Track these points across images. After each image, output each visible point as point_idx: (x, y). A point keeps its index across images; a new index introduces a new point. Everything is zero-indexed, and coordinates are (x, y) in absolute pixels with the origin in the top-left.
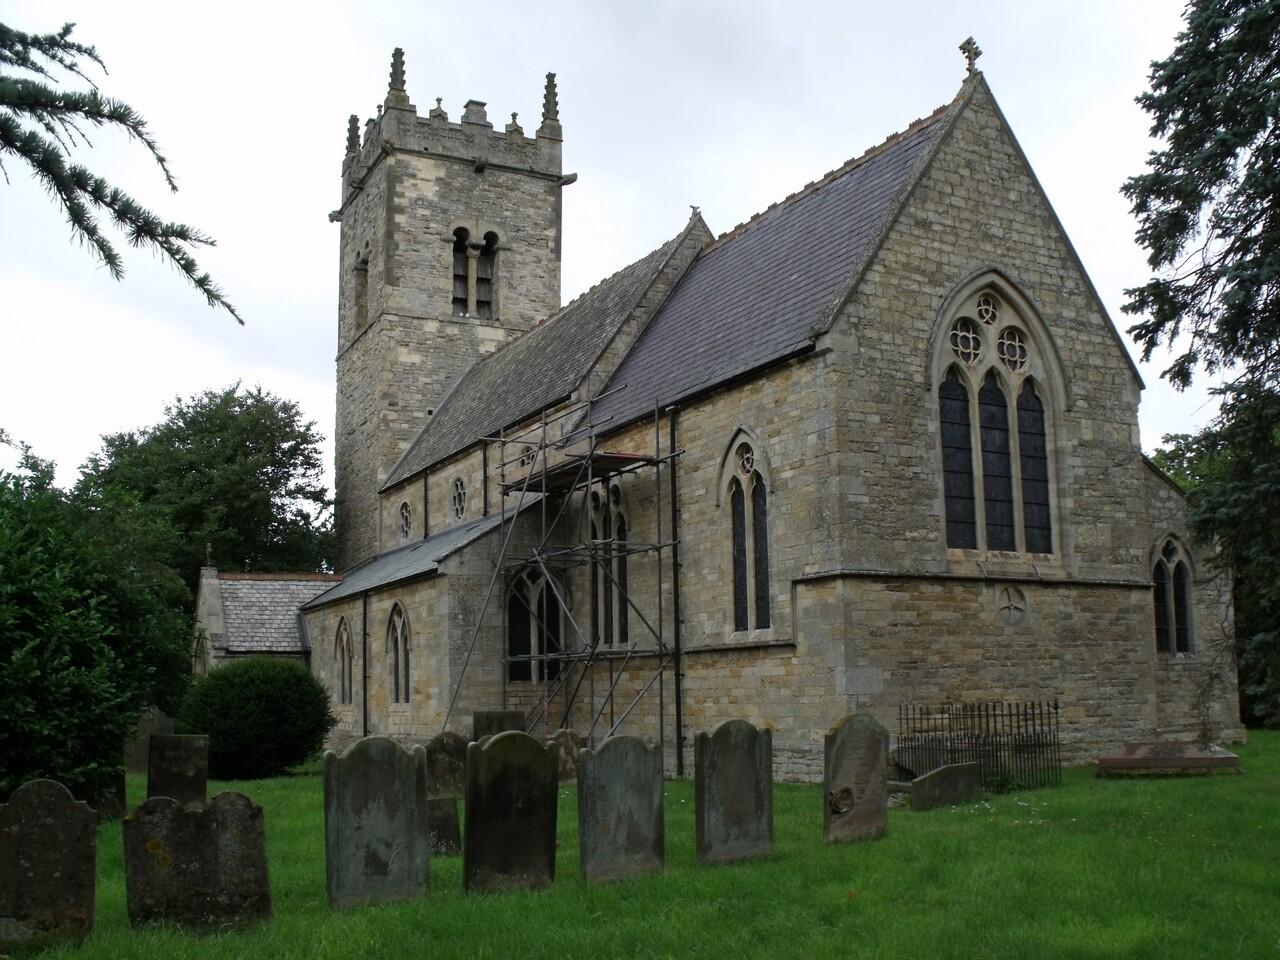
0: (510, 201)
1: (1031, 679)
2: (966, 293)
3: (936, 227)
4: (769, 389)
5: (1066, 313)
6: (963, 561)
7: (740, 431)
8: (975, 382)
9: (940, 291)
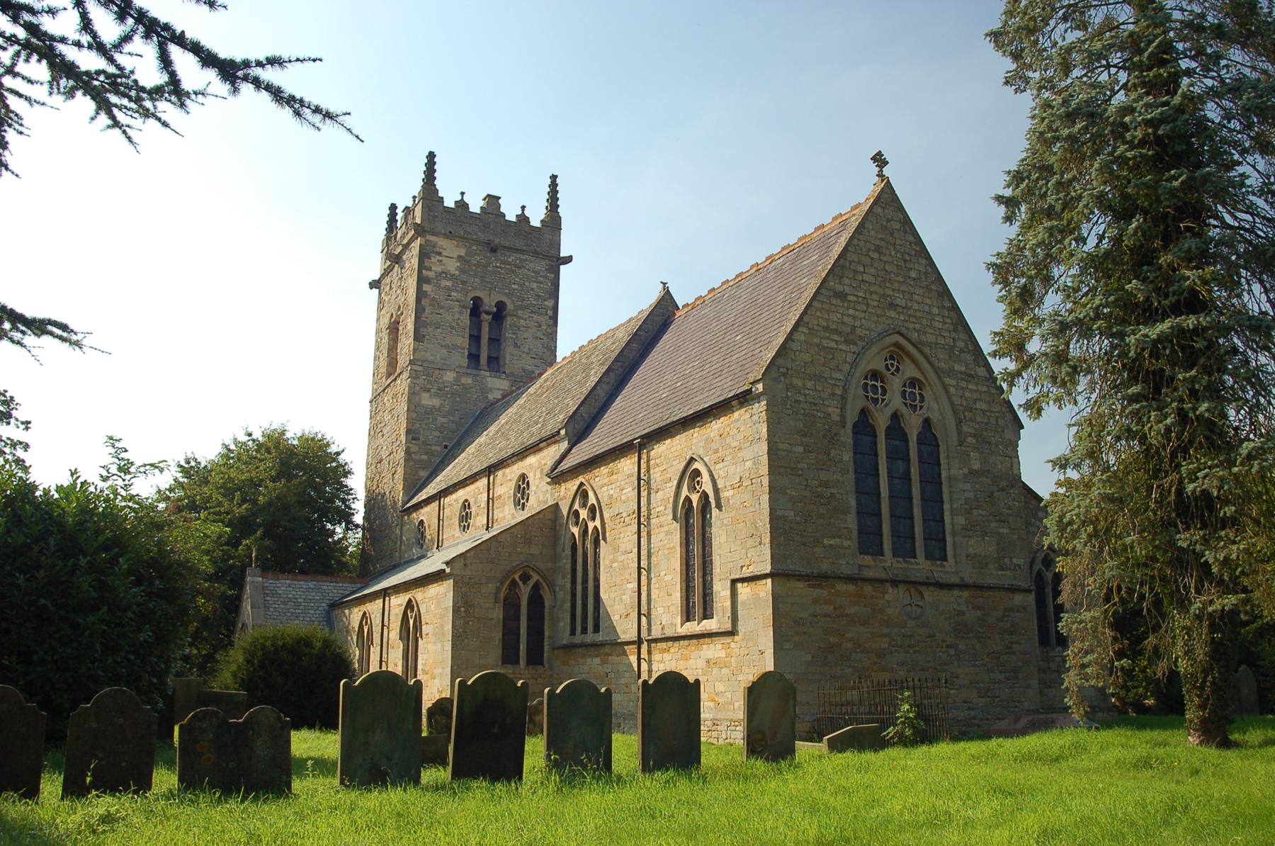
2: (874, 350)
3: (851, 298)
4: (716, 426)
5: (957, 367)
6: (872, 567)
7: (692, 460)
8: (881, 421)
9: (854, 348)
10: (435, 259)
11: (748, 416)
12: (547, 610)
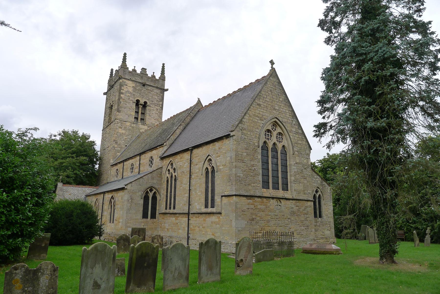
1: (283, 224)
2: (269, 123)
3: (262, 106)
8: (270, 146)
9: (263, 122)
11: (228, 142)
12: (158, 201)
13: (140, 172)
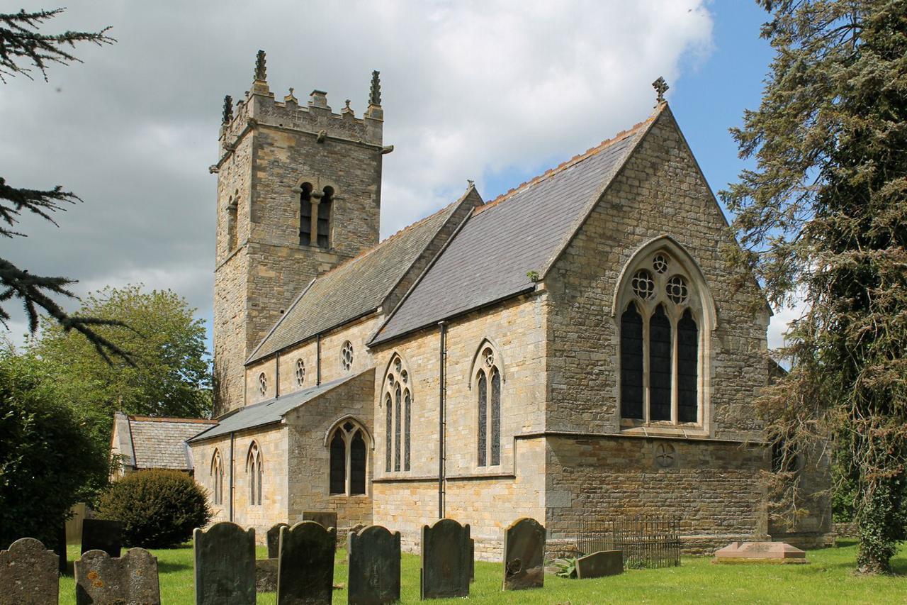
0: (343, 164)
4: (505, 315)
7: (485, 340)
10: (267, 149)
11: (531, 308)
13: (323, 382)
